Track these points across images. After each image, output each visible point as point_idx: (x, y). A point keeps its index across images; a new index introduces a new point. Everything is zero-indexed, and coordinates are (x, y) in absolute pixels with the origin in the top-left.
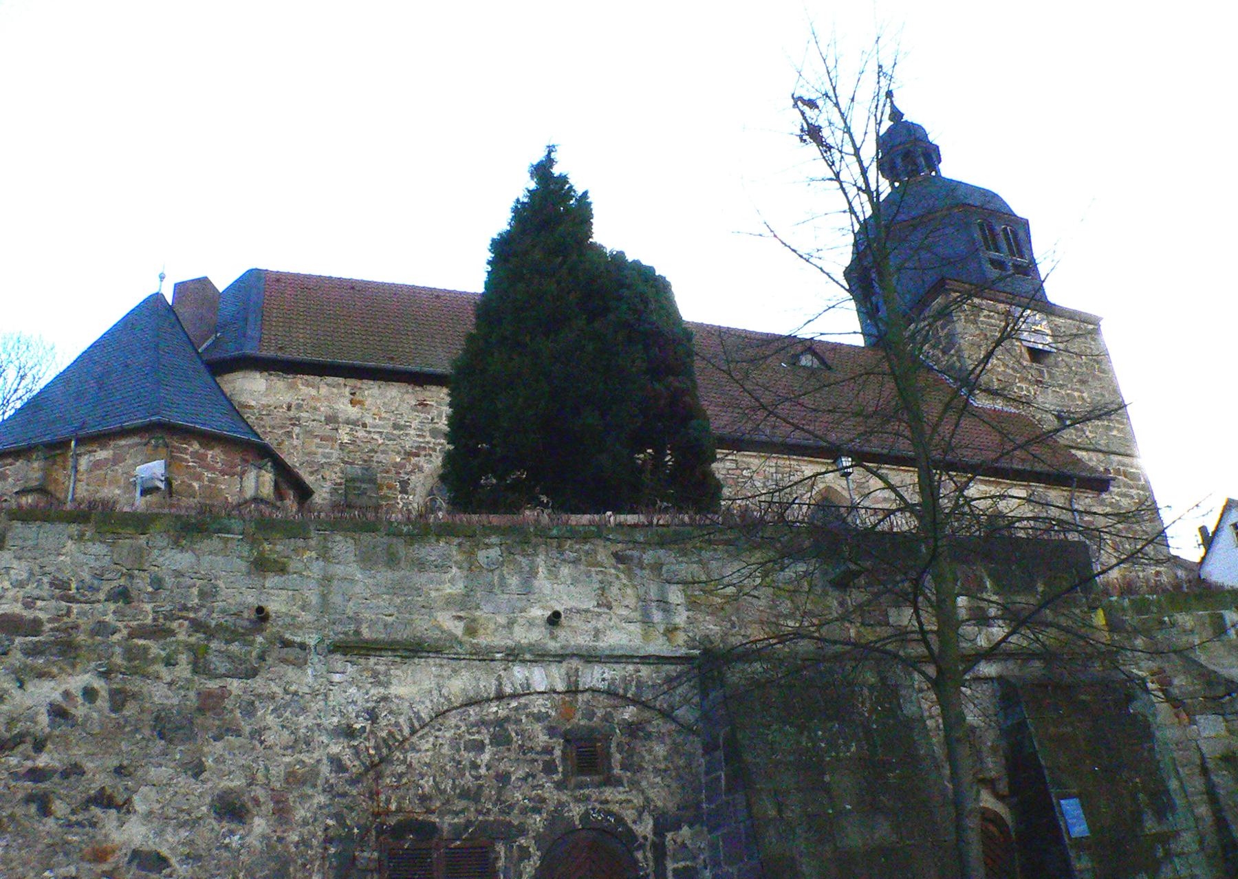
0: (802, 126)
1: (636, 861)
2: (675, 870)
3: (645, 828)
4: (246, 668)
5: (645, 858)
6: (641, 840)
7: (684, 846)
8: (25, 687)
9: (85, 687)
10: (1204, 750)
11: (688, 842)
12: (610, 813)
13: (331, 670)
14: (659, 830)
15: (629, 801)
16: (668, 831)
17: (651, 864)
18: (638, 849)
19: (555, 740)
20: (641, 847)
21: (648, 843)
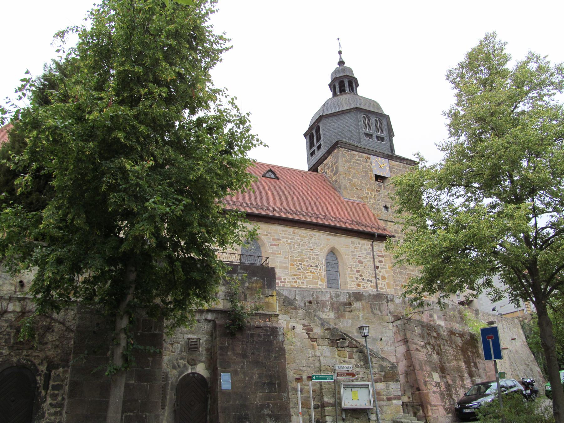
0: (212, 83)
1: (36, 380)
2: (53, 385)
3: (43, 368)
4: (87, 285)
5: (41, 379)
6: (40, 372)
7: (59, 375)
8: (421, 389)
9: (335, 248)
10: (322, 361)
11: (61, 374)
12: (29, 360)
13: (521, 311)
14: (49, 369)
15: (38, 356)
16: (53, 369)
17: (42, 382)
18: (38, 375)
19: (12, 330)
20: (40, 375)
21: (43, 374)
